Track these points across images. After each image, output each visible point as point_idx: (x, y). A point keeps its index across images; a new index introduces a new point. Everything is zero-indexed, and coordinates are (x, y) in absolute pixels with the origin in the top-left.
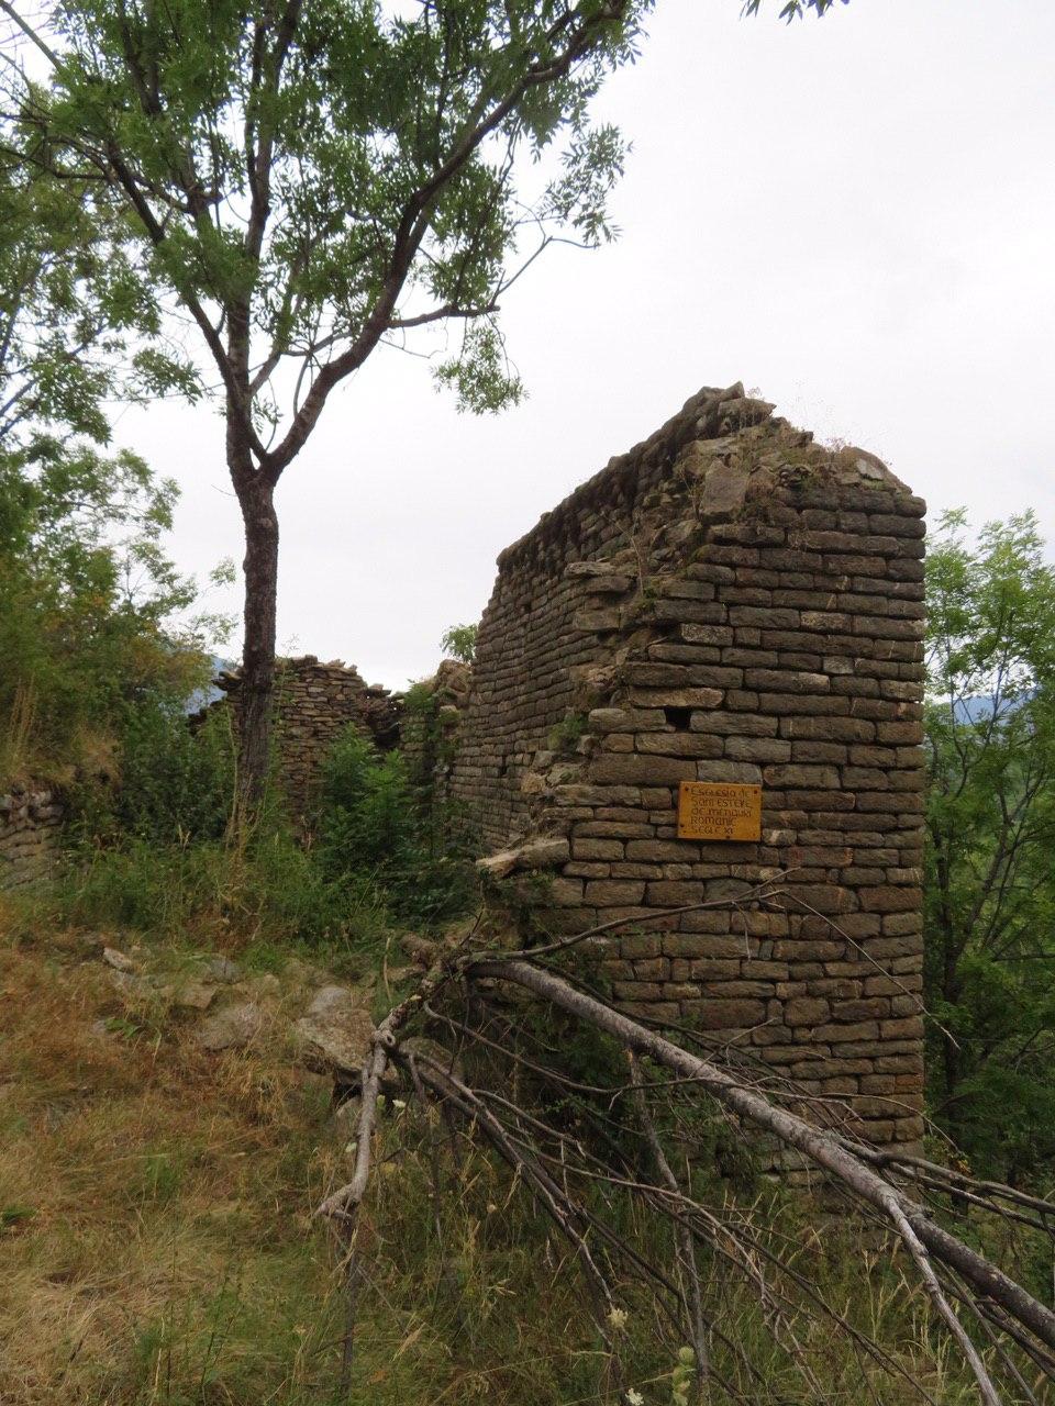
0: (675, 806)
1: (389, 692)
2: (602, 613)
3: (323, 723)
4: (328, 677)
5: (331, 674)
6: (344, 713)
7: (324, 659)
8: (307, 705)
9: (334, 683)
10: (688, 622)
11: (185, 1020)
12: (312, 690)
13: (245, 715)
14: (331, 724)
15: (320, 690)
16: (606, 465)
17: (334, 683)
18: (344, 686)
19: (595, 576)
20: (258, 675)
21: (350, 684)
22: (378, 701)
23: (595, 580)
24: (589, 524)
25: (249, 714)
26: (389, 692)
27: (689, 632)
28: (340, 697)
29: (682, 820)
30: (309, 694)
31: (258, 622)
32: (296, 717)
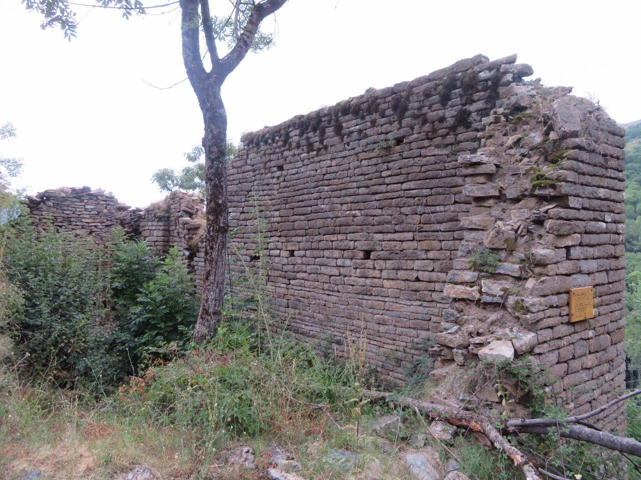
0: (568, 304)
1: (130, 207)
2: (484, 186)
3: (95, 226)
4: (98, 199)
5: (99, 197)
6: (107, 220)
7: (94, 189)
8: (85, 216)
9: (102, 202)
10: (571, 196)
11: (124, 414)
12: (88, 207)
13: (212, 248)
14: (101, 227)
15: (93, 207)
16: (393, 86)
17: (102, 202)
18: (107, 205)
19: (484, 164)
20: (222, 220)
21: (111, 203)
22: (124, 213)
23: (483, 166)
24: (351, 124)
25: (216, 247)
26: (130, 207)
27: (573, 202)
28: (105, 211)
29: (573, 312)
30: (86, 210)
31: (220, 182)
32: (78, 223)
